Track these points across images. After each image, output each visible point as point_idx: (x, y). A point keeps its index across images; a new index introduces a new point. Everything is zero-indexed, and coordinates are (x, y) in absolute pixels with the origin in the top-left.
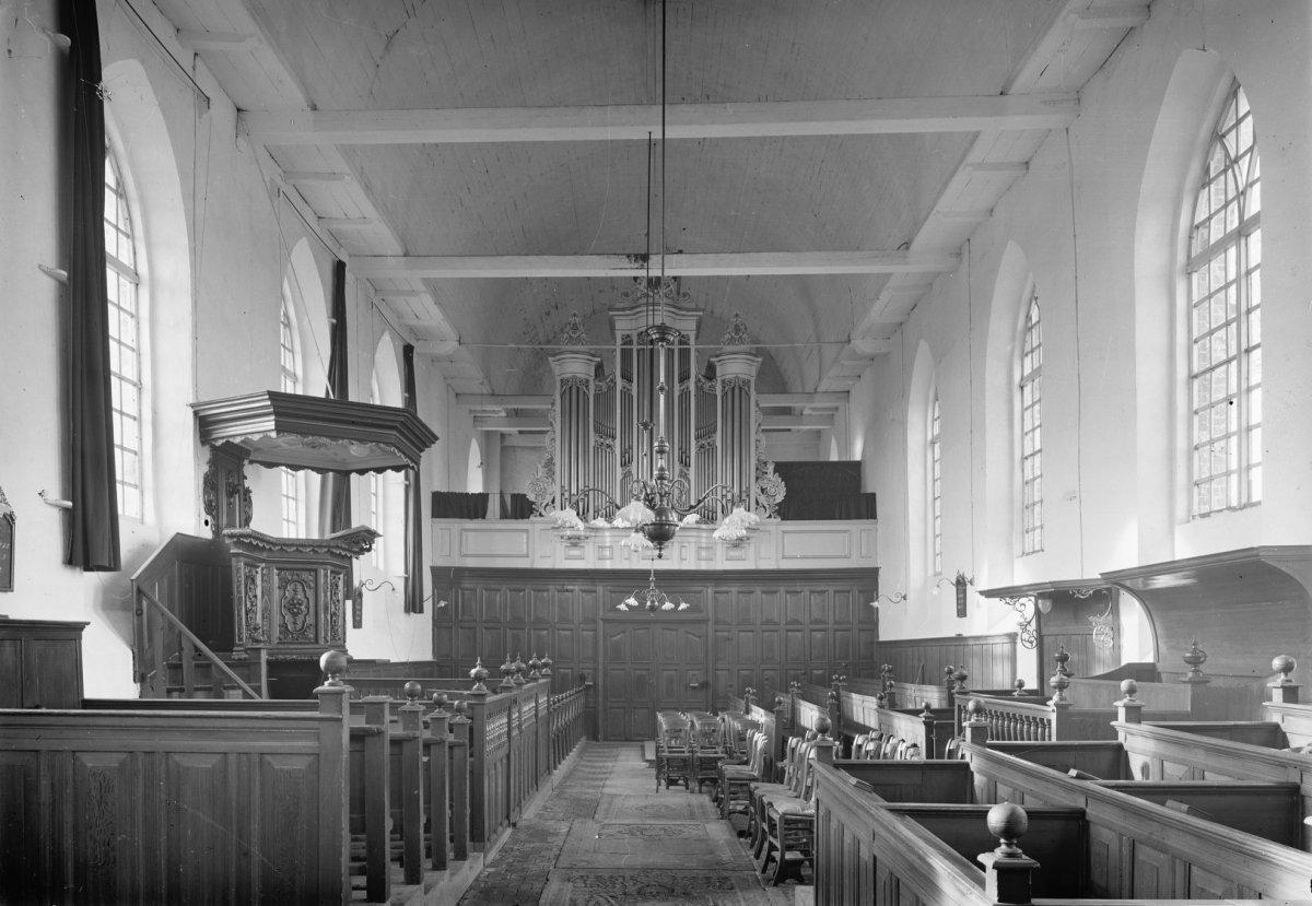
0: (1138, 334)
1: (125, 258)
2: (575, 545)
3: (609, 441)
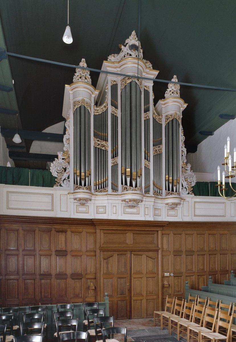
2: (83, 204)
3: (104, 143)
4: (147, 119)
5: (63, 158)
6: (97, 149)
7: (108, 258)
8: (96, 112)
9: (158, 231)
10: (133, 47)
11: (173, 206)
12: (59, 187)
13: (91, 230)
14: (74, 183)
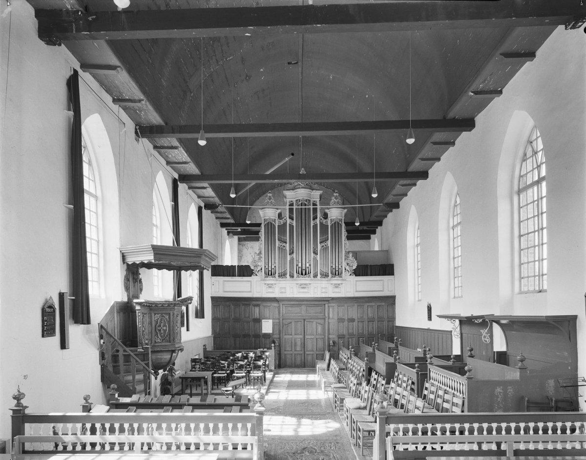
0: (498, 189)
1: (92, 191)
2: (270, 287)
3: (284, 244)
13: (276, 304)
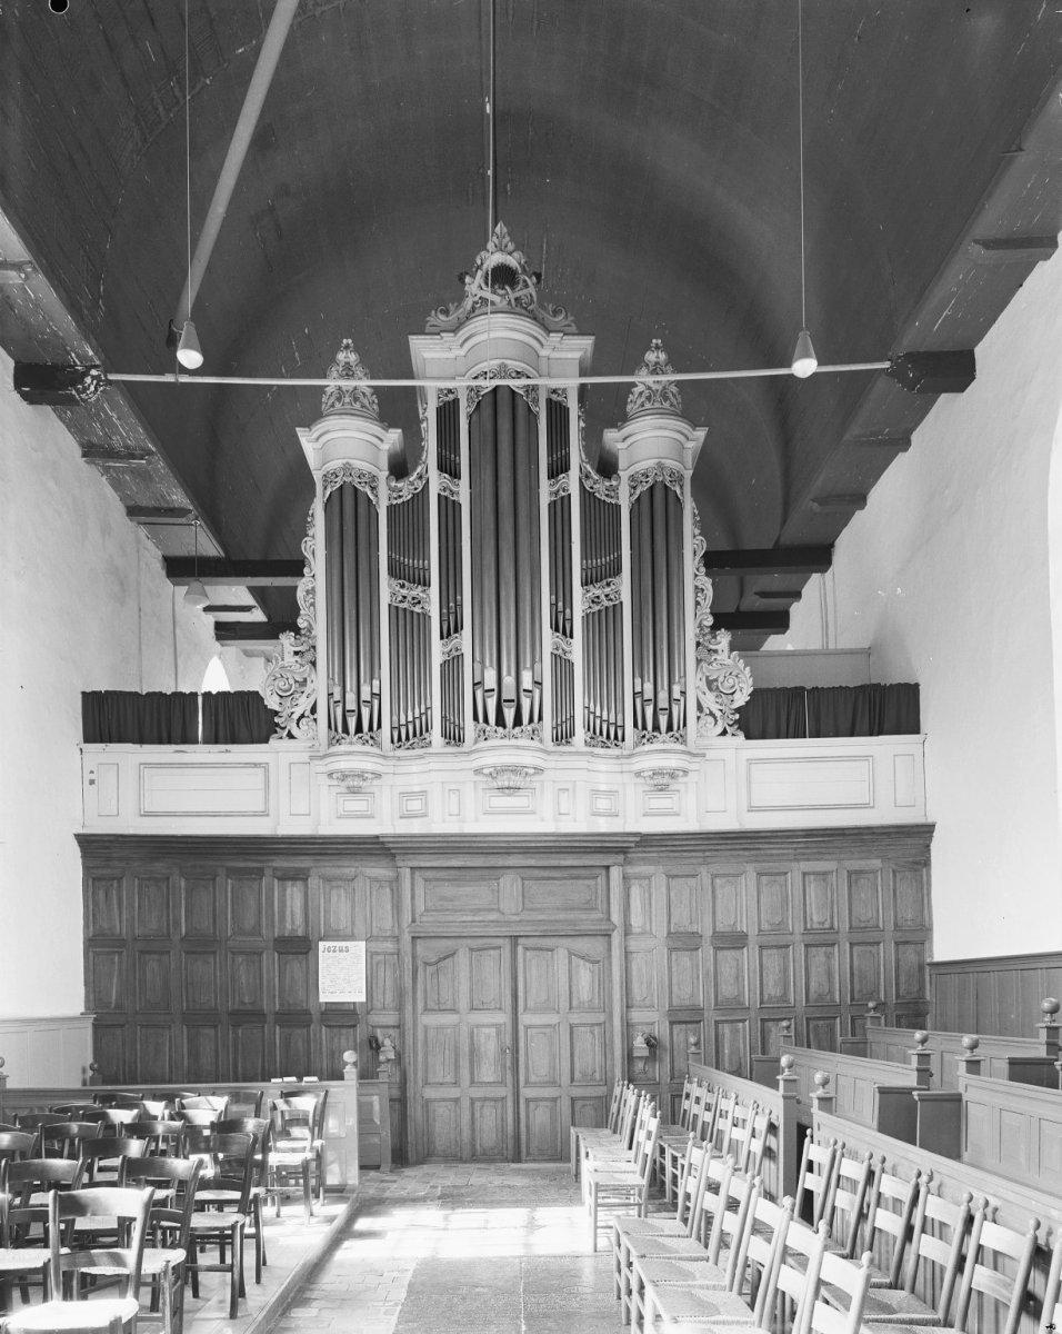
3: (417, 591)
4: (562, 498)
5: (297, 649)
6: (401, 613)
7: (440, 960)
8: (395, 495)
9: (607, 868)
10: (503, 276)
11: (659, 780)
12: (287, 742)
14: (330, 727)
